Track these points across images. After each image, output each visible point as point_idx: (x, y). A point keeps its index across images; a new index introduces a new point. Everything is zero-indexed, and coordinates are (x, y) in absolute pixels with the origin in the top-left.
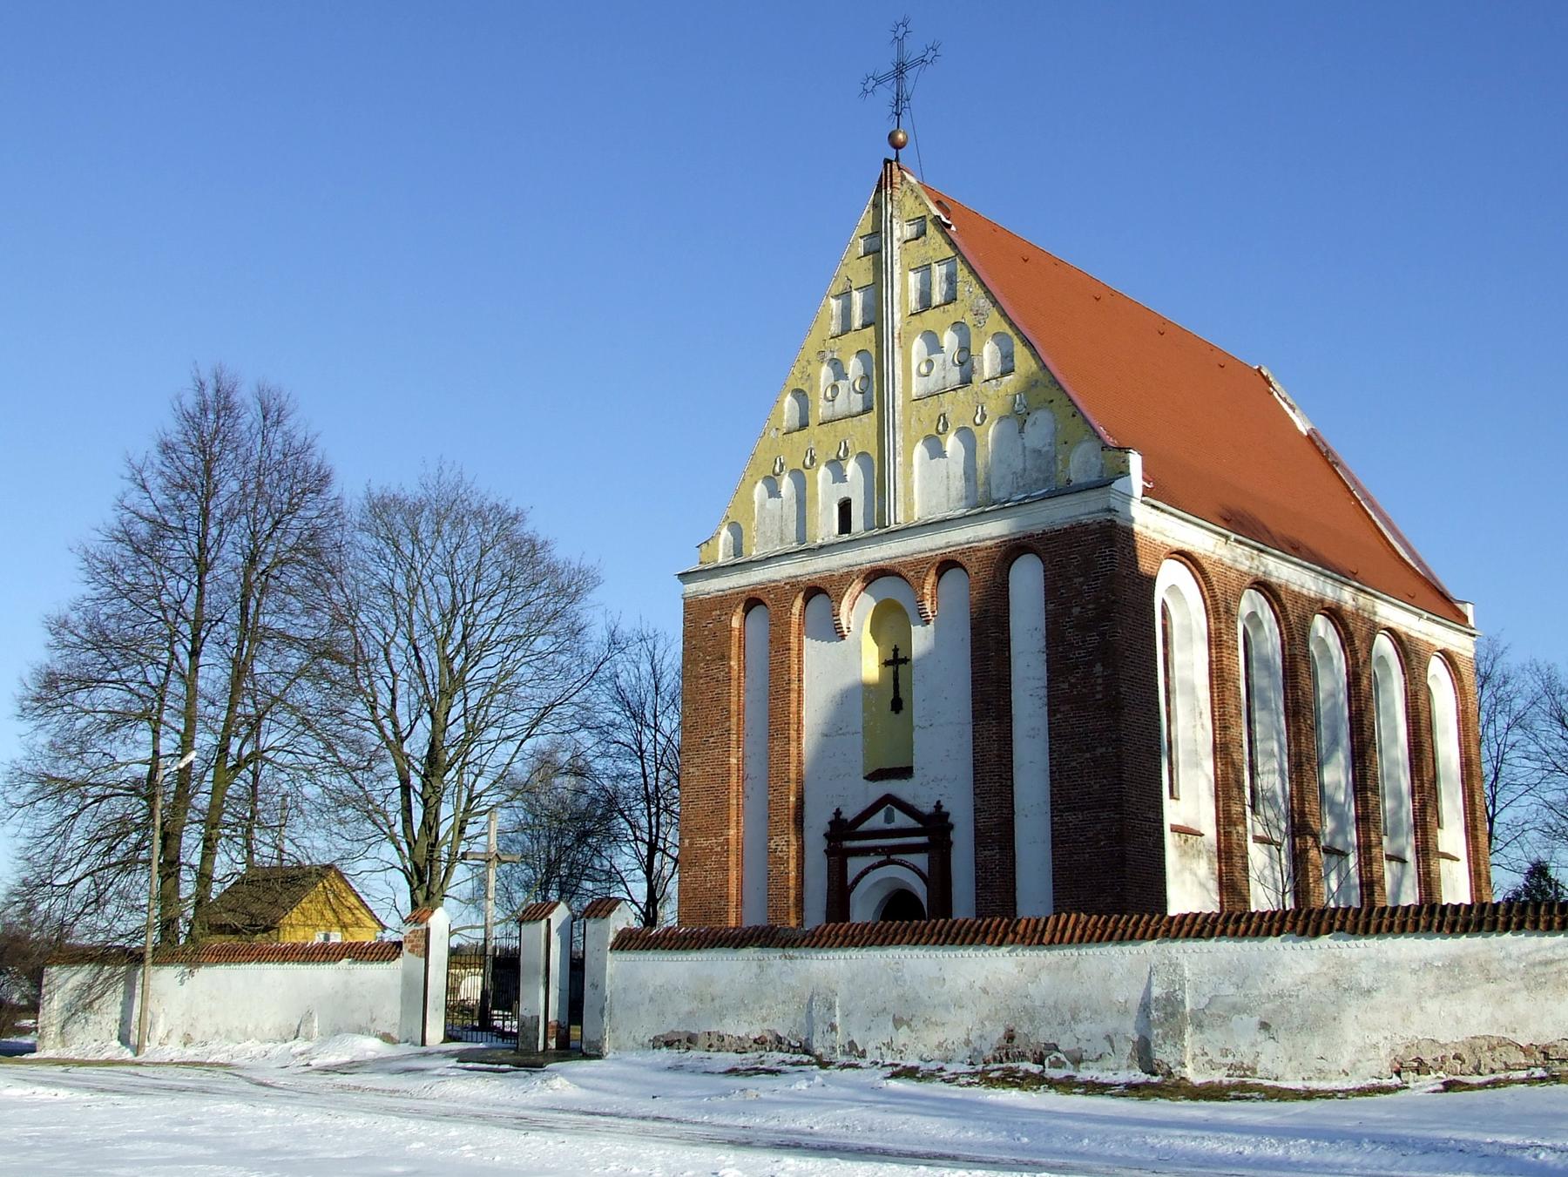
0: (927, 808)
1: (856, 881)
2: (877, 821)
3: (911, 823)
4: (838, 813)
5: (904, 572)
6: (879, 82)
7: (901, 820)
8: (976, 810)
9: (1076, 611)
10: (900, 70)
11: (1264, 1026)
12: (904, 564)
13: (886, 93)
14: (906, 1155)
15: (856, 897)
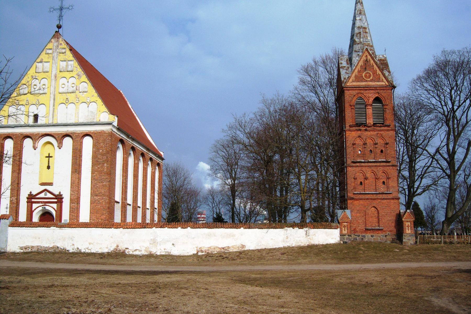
0: (57, 193)
1: (35, 209)
2: (42, 195)
3: (52, 196)
4: (31, 193)
5: (55, 136)
6: (54, 10)
7: (49, 195)
8: (71, 194)
9: (101, 151)
10: (61, 9)
11: (173, 244)
12: (55, 134)
13: (57, 13)
14: (39, 273)
15: (34, 214)
